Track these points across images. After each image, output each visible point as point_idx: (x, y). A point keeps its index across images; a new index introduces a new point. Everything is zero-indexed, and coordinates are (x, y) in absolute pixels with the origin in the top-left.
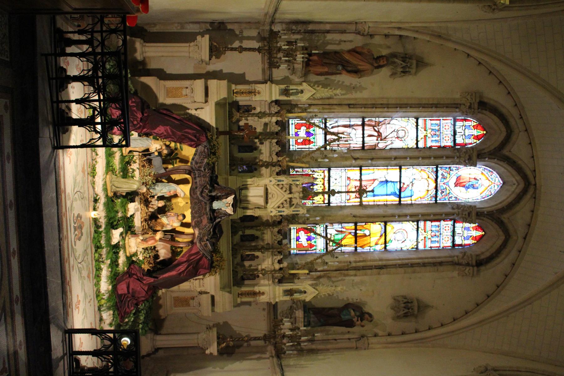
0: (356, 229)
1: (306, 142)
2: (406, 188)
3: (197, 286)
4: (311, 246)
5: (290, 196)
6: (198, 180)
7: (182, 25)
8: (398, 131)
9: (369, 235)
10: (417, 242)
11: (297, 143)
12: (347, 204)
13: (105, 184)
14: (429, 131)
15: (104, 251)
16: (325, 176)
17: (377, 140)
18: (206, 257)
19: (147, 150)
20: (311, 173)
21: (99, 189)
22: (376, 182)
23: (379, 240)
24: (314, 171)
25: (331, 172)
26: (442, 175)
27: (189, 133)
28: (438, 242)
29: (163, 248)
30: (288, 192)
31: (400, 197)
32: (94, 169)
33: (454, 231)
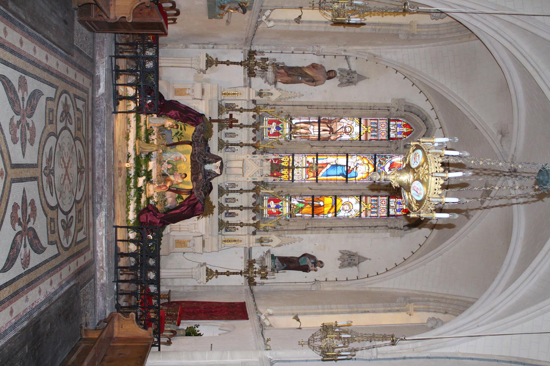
0: (313, 201)
1: (276, 134)
2: (351, 171)
3: (193, 228)
4: (280, 213)
5: (261, 168)
6: (196, 148)
7: (112, 71)
8: (345, 127)
9: (323, 206)
10: (361, 212)
11: (269, 134)
12: (306, 182)
13: (135, 146)
14: (369, 128)
15: (133, 192)
16: (290, 160)
17: (330, 134)
18: (201, 202)
19: (163, 126)
20: (280, 157)
21: (131, 150)
22: (329, 166)
23: (331, 209)
24: (281, 156)
25: (295, 157)
26: (379, 161)
27: (191, 116)
28: (376, 212)
29: (171, 197)
30: (259, 165)
31: (347, 177)
32: (128, 136)
33: (388, 205)
